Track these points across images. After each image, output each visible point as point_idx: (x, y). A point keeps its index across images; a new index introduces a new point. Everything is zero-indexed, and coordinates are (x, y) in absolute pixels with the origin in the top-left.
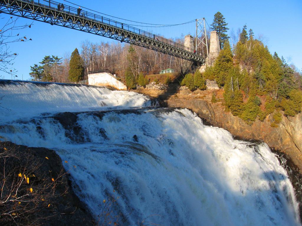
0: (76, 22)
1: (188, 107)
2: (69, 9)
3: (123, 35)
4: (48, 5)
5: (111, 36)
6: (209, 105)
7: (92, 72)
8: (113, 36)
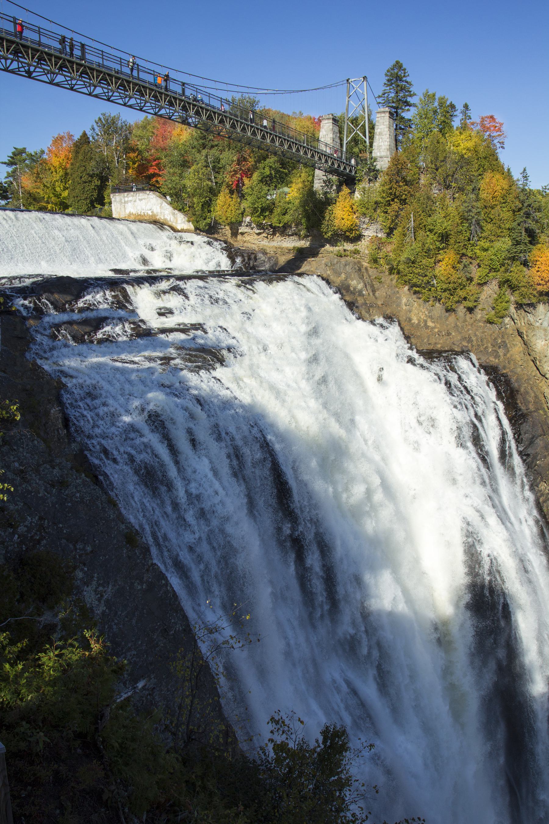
0: (79, 74)
1: (319, 274)
2: (121, 65)
3: (184, 109)
4: (152, 81)
5: (159, 111)
6: (363, 270)
7: (118, 190)
8: (163, 112)
